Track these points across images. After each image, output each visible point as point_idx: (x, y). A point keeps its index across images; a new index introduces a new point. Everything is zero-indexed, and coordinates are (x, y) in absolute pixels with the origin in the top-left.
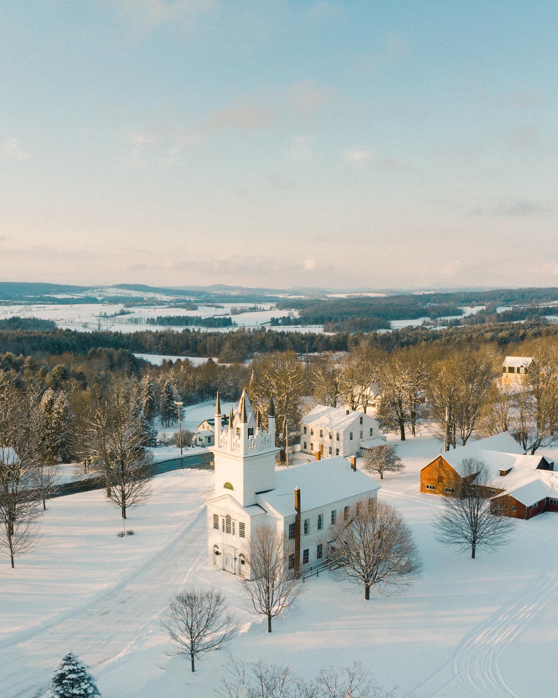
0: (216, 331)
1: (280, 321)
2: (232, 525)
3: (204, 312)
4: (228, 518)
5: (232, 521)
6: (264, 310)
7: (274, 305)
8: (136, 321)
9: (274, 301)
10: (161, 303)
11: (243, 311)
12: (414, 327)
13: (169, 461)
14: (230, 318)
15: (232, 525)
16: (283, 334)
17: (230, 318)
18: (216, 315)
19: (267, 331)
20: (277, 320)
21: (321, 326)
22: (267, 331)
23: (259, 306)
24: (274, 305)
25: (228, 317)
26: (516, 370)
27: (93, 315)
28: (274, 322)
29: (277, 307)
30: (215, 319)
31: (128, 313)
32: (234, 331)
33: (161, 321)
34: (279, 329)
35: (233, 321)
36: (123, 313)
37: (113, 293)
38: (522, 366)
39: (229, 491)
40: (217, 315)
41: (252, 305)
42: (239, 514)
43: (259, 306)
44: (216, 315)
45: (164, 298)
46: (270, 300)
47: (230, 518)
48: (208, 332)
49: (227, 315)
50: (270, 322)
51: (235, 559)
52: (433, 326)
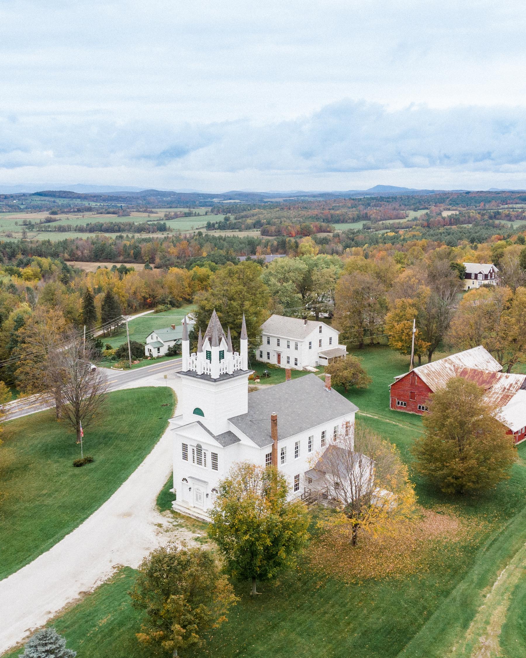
0: (246, 235)
1: (216, 226)
2: (203, 456)
3: (138, 218)
4: (199, 449)
5: (203, 452)
6: (199, 215)
7: (209, 209)
8: (61, 229)
9: (210, 206)
10: (89, 209)
11: (176, 216)
12: (355, 231)
13: (133, 380)
14: (165, 223)
15: (203, 456)
16: (220, 238)
17: (165, 223)
18: (149, 221)
19: (204, 236)
20: (214, 225)
21: (258, 230)
22: (204, 236)
23: (194, 211)
24: (209, 209)
25: (162, 222)
26: (473, 276)
27: (16, 223)
28: (210, 227)
29: (212, 211)
30: (149, 225)
31: (55, 220)
32: (169, 236)
33: (91, 229)
34: (217, 234)
35: (167, 226)
36: (49, 221)
37: (38, 201)
38: (480, 273)
39: (198, 418)
40: (151, 221)
41: (186, 210)
42: (510, 575)
43: (194, 211)
44: (149, 221)
45: (93, 204)
46: (205, 205)
47: (201, 447)
48: (143, 237)
49: (160, 220)
50: (206, 227)
51: (207, 495)
52: (389, 231)
